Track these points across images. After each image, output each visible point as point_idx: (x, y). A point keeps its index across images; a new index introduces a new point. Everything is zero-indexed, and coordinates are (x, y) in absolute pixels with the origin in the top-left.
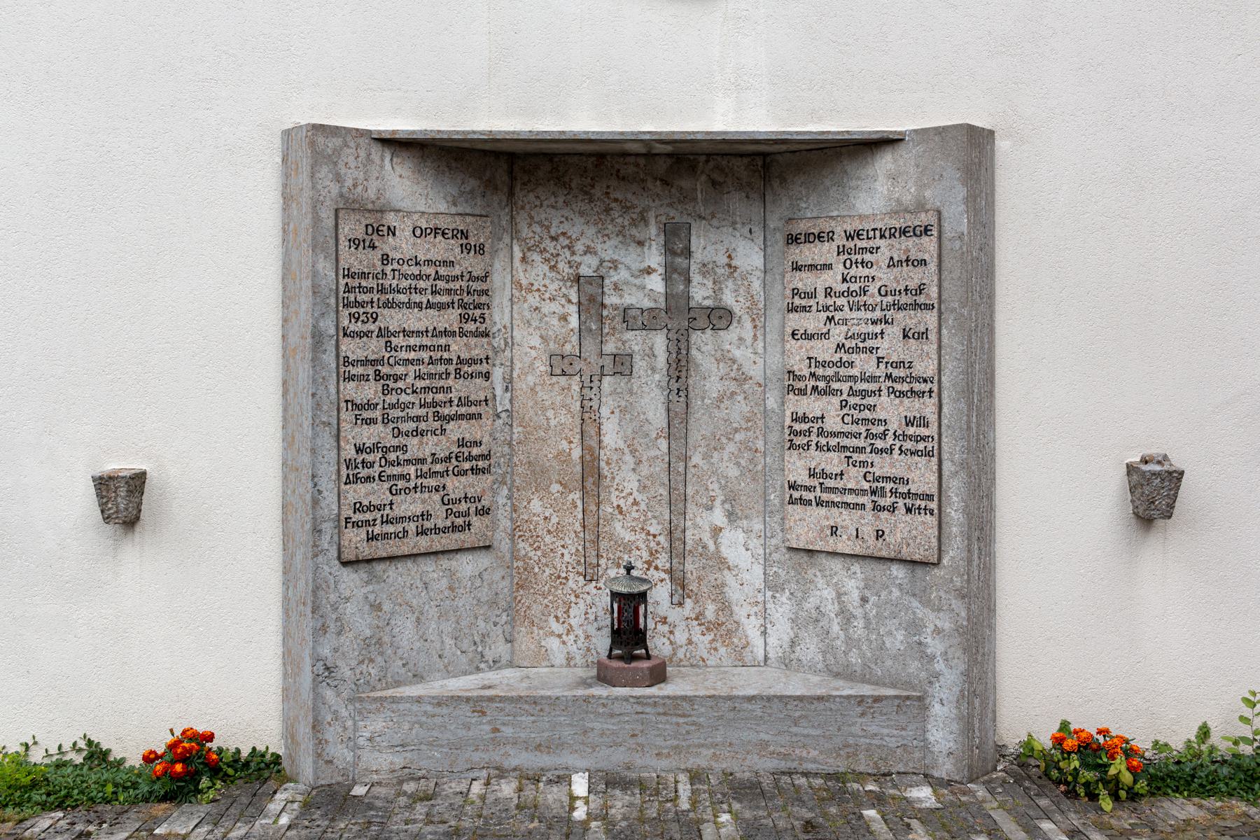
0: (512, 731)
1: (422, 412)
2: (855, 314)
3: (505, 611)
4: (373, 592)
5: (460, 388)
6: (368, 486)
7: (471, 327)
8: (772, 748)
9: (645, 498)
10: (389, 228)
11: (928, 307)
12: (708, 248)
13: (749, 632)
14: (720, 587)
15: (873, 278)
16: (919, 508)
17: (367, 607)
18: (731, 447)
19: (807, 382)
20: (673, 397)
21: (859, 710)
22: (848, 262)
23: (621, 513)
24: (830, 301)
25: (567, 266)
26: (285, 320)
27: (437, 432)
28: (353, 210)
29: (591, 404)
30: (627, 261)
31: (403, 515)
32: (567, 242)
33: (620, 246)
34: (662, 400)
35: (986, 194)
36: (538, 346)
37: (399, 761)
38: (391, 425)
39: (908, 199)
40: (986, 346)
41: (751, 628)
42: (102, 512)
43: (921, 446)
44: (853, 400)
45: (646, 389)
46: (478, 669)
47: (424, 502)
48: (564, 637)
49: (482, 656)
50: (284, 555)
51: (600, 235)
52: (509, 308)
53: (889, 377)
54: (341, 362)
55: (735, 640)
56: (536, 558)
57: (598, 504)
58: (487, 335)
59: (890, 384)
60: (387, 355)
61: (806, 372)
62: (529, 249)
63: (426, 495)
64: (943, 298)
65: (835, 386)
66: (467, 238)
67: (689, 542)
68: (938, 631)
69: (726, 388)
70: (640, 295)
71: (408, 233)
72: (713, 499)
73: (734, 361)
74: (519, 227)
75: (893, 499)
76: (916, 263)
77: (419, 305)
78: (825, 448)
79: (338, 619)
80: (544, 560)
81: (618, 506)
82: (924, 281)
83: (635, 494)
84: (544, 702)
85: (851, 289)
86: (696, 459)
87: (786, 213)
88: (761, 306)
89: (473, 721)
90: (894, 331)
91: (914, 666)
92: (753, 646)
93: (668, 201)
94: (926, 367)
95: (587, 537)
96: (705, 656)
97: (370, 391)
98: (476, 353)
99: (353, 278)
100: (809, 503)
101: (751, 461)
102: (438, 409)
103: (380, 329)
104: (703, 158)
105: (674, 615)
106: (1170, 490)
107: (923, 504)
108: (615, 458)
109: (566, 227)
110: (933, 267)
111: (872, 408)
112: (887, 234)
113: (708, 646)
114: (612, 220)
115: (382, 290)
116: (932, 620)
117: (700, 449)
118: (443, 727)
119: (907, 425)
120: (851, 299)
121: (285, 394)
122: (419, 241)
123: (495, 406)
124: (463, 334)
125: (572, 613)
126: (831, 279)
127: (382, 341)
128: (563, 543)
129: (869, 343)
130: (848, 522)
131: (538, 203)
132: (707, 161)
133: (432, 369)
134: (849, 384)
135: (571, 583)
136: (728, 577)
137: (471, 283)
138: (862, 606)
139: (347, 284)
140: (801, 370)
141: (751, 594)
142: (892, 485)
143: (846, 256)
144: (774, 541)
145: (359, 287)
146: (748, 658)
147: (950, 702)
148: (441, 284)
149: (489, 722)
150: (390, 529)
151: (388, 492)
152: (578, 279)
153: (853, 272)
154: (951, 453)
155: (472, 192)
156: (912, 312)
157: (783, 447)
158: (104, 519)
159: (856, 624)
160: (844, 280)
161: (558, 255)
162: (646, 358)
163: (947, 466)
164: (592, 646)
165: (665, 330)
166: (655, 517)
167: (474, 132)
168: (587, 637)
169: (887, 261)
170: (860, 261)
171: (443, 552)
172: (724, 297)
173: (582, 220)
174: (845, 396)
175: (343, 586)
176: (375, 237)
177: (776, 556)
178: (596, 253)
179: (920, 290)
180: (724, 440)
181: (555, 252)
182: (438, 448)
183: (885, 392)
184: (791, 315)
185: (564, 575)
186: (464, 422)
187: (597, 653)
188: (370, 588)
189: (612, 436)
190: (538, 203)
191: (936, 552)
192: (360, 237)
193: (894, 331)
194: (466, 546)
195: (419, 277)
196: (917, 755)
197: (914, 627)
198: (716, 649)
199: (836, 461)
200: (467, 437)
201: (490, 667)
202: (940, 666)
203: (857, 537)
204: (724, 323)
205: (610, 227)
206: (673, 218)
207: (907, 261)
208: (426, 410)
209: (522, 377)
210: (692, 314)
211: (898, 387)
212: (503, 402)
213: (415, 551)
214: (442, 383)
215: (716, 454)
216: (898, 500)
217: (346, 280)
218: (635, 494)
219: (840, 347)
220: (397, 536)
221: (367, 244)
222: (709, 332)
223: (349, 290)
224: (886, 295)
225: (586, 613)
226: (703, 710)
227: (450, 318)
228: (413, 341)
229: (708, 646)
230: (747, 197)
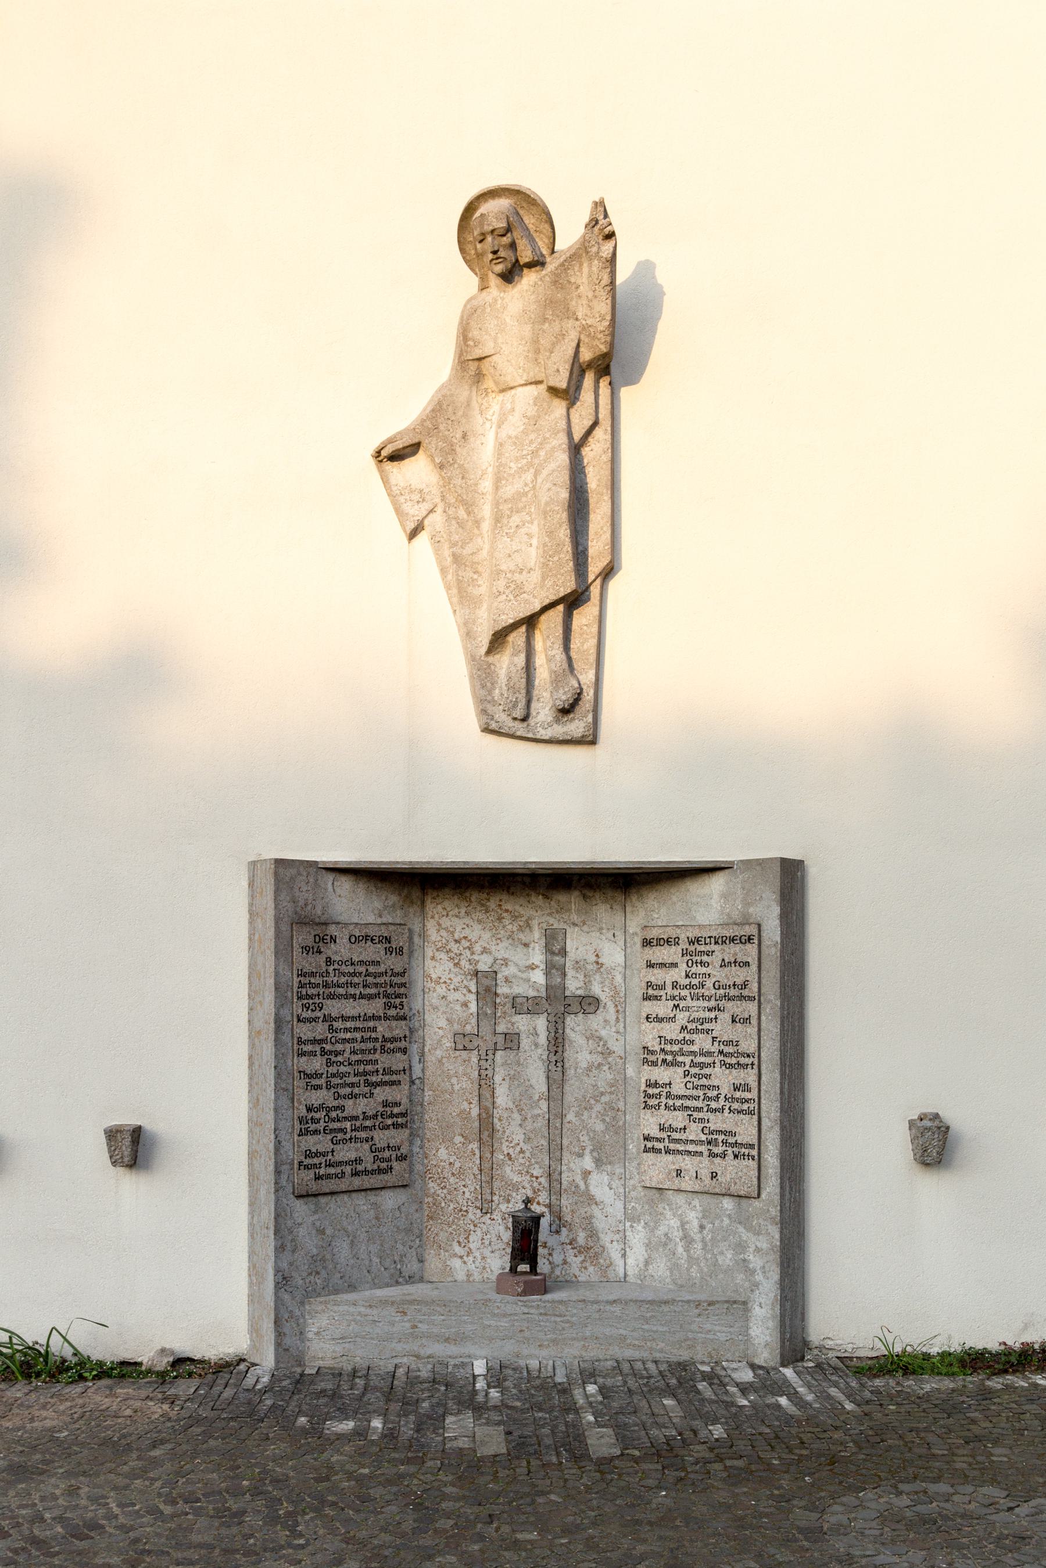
0: (427, 1327)
1: (355, 1080)
2: (695, 1003)
3: (417, 1237)
4: (319, 1220)
5: (384, 1061)
6: (316, 1137)
7: (392, 1012)
8: (628, 1341)
9: (529, 1148)
10: (331, 937)
11: (751, 999)
12: (580, 949)
13: (612, 1255)
15: (709, 975)
16: (744, 1155)
17: (314, 1232)
19: (658, 1056)
20: (552, 1067)
21: (697, 1311)
22: (690, 962)
23: (510, 1159)
24: (676, 992)
25: (468, 963)
26: (251, 1009)
27: (367, 1096)
28: (305, 924)
29: (486, 1073)
30: (515, 959)
31: (341, 1160)
32: (468, 944)
33: (510, 947)
34: (543, 1070)
35: (797, 910)
36: (444, 1026)
37: (339, 1349)
38: (333, 1090)
39: (736, 916)
40: (797, 1029)
41: (614, 1251)
42: (111, 1157)
43: (745, 1106)
44: (693, 1071)
45: (530, 1061)
46: (397, 1283)
47: (357, 1150)
48: (465, 1258)
49: (401, 1273)
50: (249, 1191)
51: (494, 939)
52: (422, 997)
53: (721, 1052)
54: (295, 1042)
55: (601, 1261)
56: (443, 1195)
57: (492, 1153)
58: (405, 1019)
59: (721, 1058)
60: (330, 1036)
62: (437, 950)
63: (359, 1145)
64: (762, 992)
65: (680, 1059)
66: (390, 943)
67: (565, 1183)
69: (594, 1060)
70: (526, 986)
71: (346, 940)
72: (583, 1148)
73: (600, 1039)
74: (429, 933)
75: (724, 1148)
76: (741, 964)
77: (353, 996)
78: (672, 1108)
79: (293, 1240)
80: (449, 1197)
81: (508, 1154)
82: (748, 979)
83: (522, 1144)
84: (452, 1304)
85: (692, 983)
86: (570, 1117)
87: (642, 922)
88: (622, 995)
89: (397, 1319)
91: (740, 1277)
92: (616, 1266)
93: (549, 911)
94: (749, 1045)
95: (483, 1178)
96: (577, 1273)
97: (317, 1064)
98: (400, 1033)
99: (305, 976)
100: (659, 1151)
101: (614, 1118)
102: (368, 1077)
103: (325, 1015)
104: (576, 878)
105: (552, 1241)
106: (940, 1141)
107: (747, 1151)
108: (505, 1115)
109: (467, 932)
110: (754, 967)
111: (708, 1076)
112: (720, 942)
113: (579, 1265)
114: (504, 927)
115: (326, 985)
117: (573, 1109)
119: (735, 1090)
120: (693, 991)
121: (251, 1065)
122: (353, 946)
123: (411, 1074)
124: (387, 1018)
125: (471, 1239)
126: (676, 975)
127: (326, 1025)
128: (464, 1183)
129: (706, 1026)
130: (689, 1166)
131: (445, 913)
132: (579, 880)
133: (363, 1046)
134: (691, 1058)
135: (470, 1215)
136: (596, 1211)
137: (393, 978)
138: (701, 1232)
139: (300, 981)
140: (653, 1046)
141: (613, 1224)
142: (723, 1137)
143: (689, 957)
144: (632, 1182)
145: (310, 983)
146: (611, 1275)
147: (767, 1305)
148: (370, 980)
149: (409, 1321)
150: (332, 1171)
151: (330, 1143)
153: (694, 970)
154: (768, 1112)
155: (393, 906)
156: (739, 1002)
157: (639, 1107)
158: (112, 1163)
159: (696, 1246)
160: (687, 976)
161: (461, 954)
162: (531, 1036)
163: (765, 1123)
164: (487, 1266)
165: (546, 1014)
166: (537, 1163)
167: (398, 863)
168: (483, 1258)
169: (720, 962)
170: (699, 961)
171: (371, 1189)
172: (593, 988)
173: (480, 927)
174: (687, 1067)
175: (297, 1215)
176: (321, 944)
178: (490, 953)
179: (745, 985)
180: (592, 1102)
181: (458, 952)
182: (368, 1108)
183: (718, 1064)
184: (646, 1003)
185: (464, 1209)
186: (387, 1088)
187: (491, 1271)
188: (316, 1217)
189: (503, 1098)
190: (445, 913)
191: (756, 1189)
192: (310, 945)
194: (389, 1185)
195: (354, 974)
196: (742, 1347)
198: (586, 1268)
199: (680, 1119)
200: (390, 1099)
201: (407, 1282)
203: (697, 1177)
204: (592, 1009)
205: (502, 932)
206: (552, 925)
207: (735, 962)
208: (359, 1078)
209: (433, 1051)
210: (567, 1002)
211: (728, 1060)
212: (417, 1072)
213: (350, 1188)
214: (371, 1057)
215: (586, 1113)
216: (727, 1148)
217: (300, 978)
218: (522, 1144)
219: (683, 1028)
220: (336, 1176)
221: (315, 950)
222: (580, 1015)
223: (301, 985)
224: (719, 988)
225: (483, 1239)
226: (575, 1311)
227: (376, 1007)
228: (348, 1025)
229: (579, 1265)
230: (611, 908)
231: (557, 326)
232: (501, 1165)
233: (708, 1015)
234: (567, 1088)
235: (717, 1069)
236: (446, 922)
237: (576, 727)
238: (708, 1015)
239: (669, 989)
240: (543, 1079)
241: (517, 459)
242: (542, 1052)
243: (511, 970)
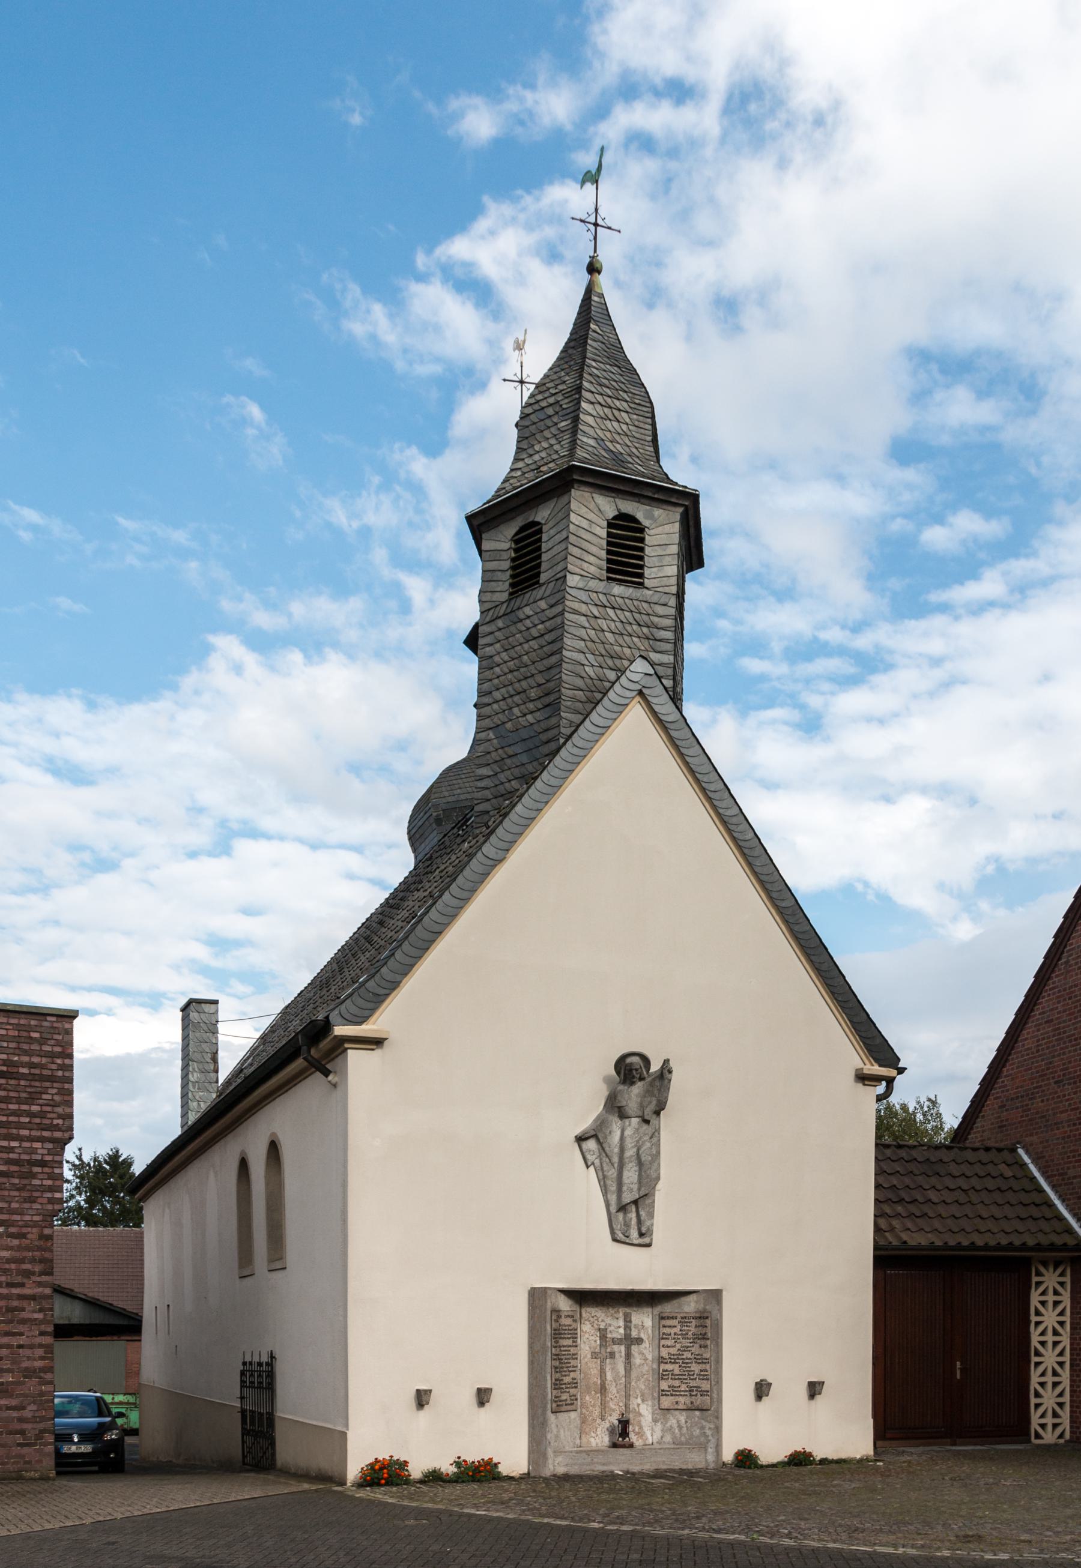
14: (639, 1422)
18: (643, 1380)
41: (648, 1434)
44: (683, 1365)
61: (667, 1357)
68: (710, 1428)
86: (633, 1383)
90: (697, 1346)
91: (702, 1439)
110: (709, 1328)
111: (690, 1367)
116: (708, 1425)
118: (578, 1459)
126: (677, 1330)
129: (689, 1349)
152: (599, 1329)
153: (683, 1328)
177: (656, 1412)
179: (705, 1334)
189: (609, 1376)
193: (697, 1346)
197: (702, 1428)
202: (710, 1438)
219: (679, 1350)
231: (649, 1099)
232: (609, 1402)
233: (689, 1345)
234: (632, 1373)
235: (694, 1364)
236: (589, 1309)
237: (646, 1240)
238: (689, 1345)
239: (673, 1336)
240: (623, 1369)
241: (631, 1143)
242: (623, 1359)
243: (611, 1328)
